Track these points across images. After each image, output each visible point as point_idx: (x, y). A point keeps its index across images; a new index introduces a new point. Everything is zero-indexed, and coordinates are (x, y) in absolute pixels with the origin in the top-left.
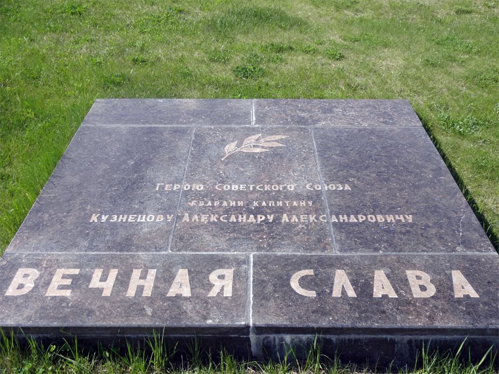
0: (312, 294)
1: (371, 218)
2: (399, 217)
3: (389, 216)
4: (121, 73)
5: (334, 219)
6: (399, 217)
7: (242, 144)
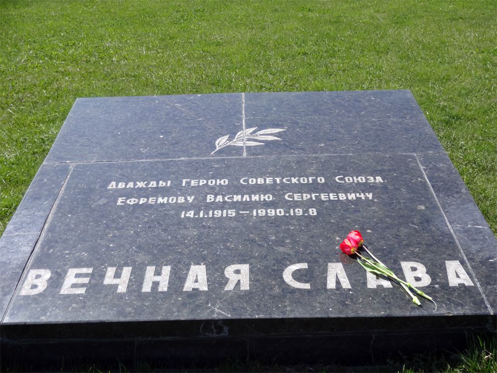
0: (307, 286)
2: (360, 195)
3: (352, 198)
4: (433, 237)
6: (360, 195)
7: (234, 138)
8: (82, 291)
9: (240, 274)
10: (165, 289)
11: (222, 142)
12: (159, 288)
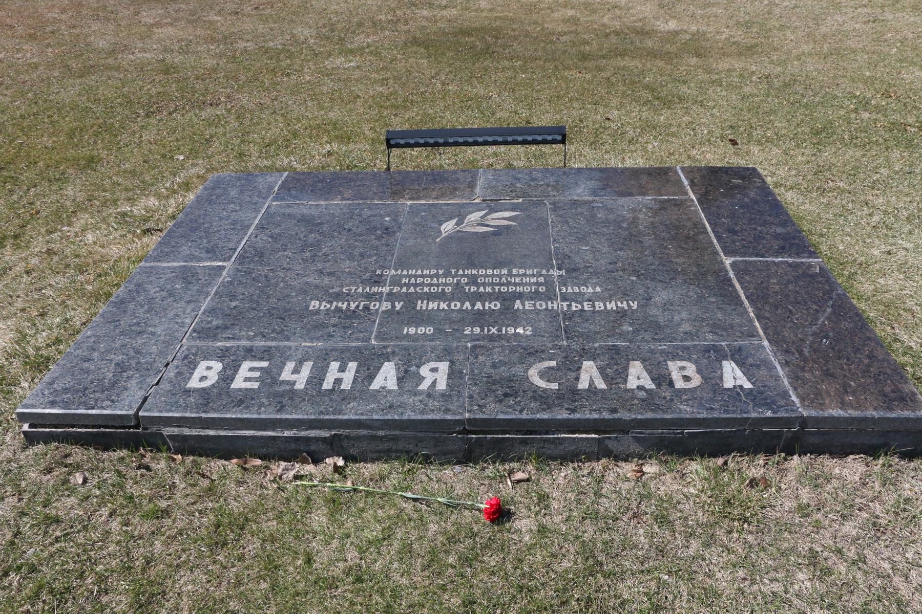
0: (554, 386)
1: (541, 305)
8: (255, 385)
10: (555, 362)
11: (448, 227)
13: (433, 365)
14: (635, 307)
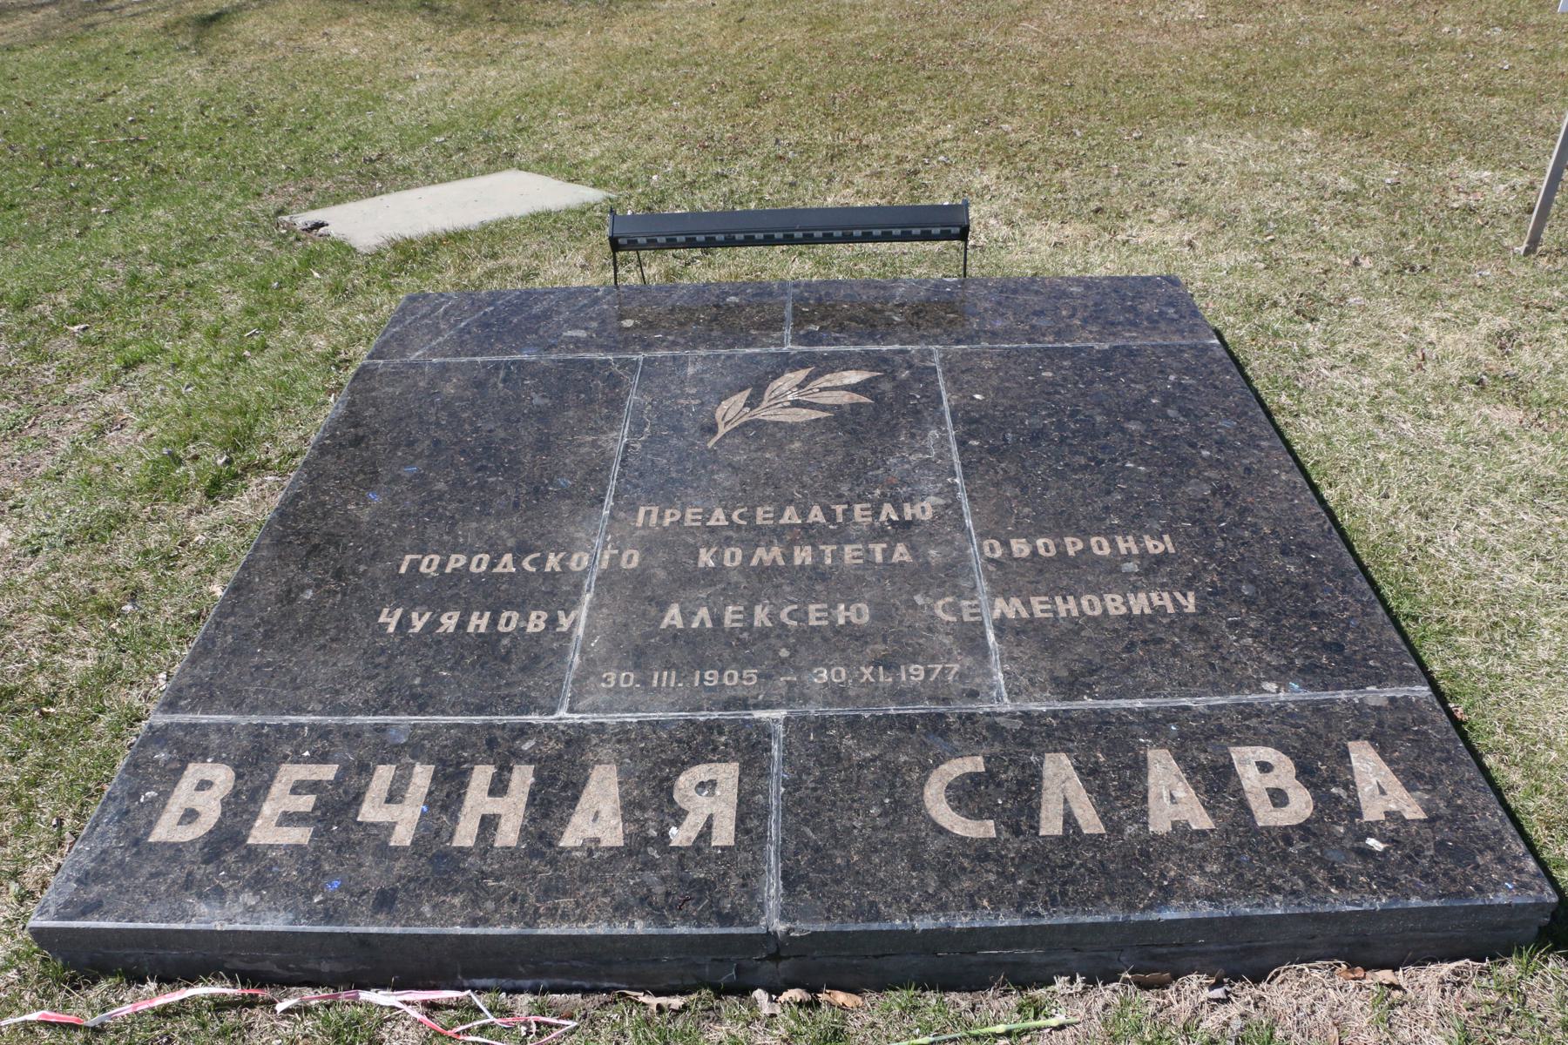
5: (1009, 608)
8: (300, 835)
9: (499, 816)
10: (418, 768)
11: (732, 410)
12: (567, 835)
13: (701, 772)
14: (1191, 609)
